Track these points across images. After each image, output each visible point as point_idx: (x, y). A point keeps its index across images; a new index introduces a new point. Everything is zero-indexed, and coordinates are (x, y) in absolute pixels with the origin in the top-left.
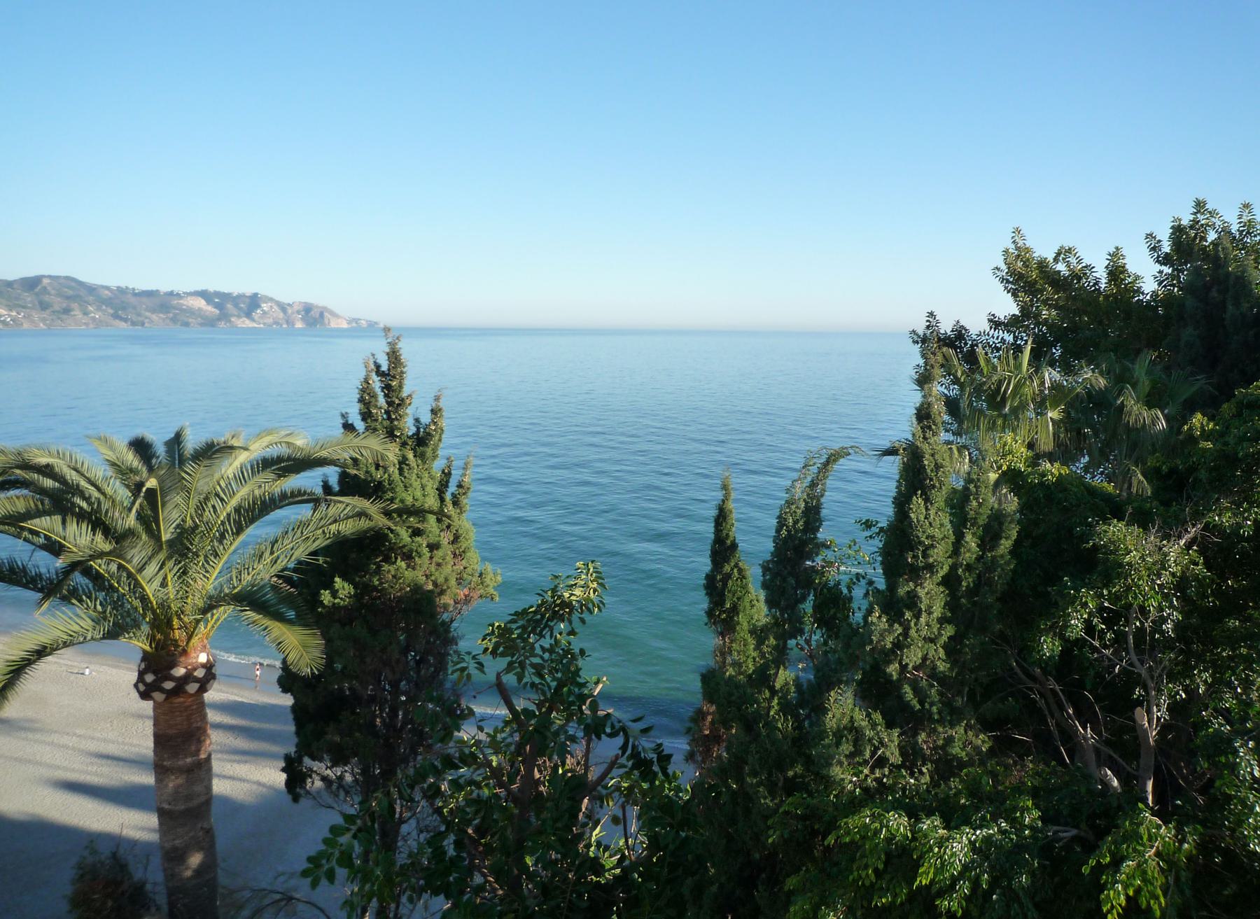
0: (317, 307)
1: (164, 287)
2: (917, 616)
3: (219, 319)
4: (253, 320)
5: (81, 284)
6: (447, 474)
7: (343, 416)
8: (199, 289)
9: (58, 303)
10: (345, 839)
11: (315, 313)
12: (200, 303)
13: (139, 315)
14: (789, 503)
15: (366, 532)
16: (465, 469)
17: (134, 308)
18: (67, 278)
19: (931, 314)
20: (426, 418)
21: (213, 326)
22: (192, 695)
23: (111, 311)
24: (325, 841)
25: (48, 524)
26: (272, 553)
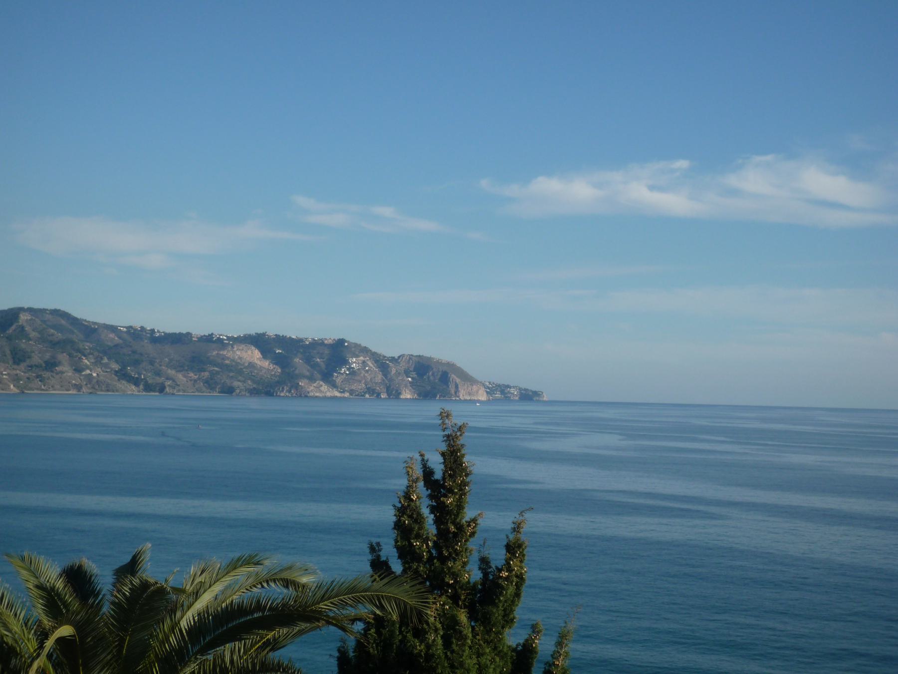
0: (439, 363)
1: (198, 327)
3: (280, 383)
4: (334, 385)
5: (75, 321)
8: (253, 331)
12: (253, 355)
13: (158, 373)
18: (56, 312)
20: (498, 556)
21: (269, 394)
23: (115, 366)
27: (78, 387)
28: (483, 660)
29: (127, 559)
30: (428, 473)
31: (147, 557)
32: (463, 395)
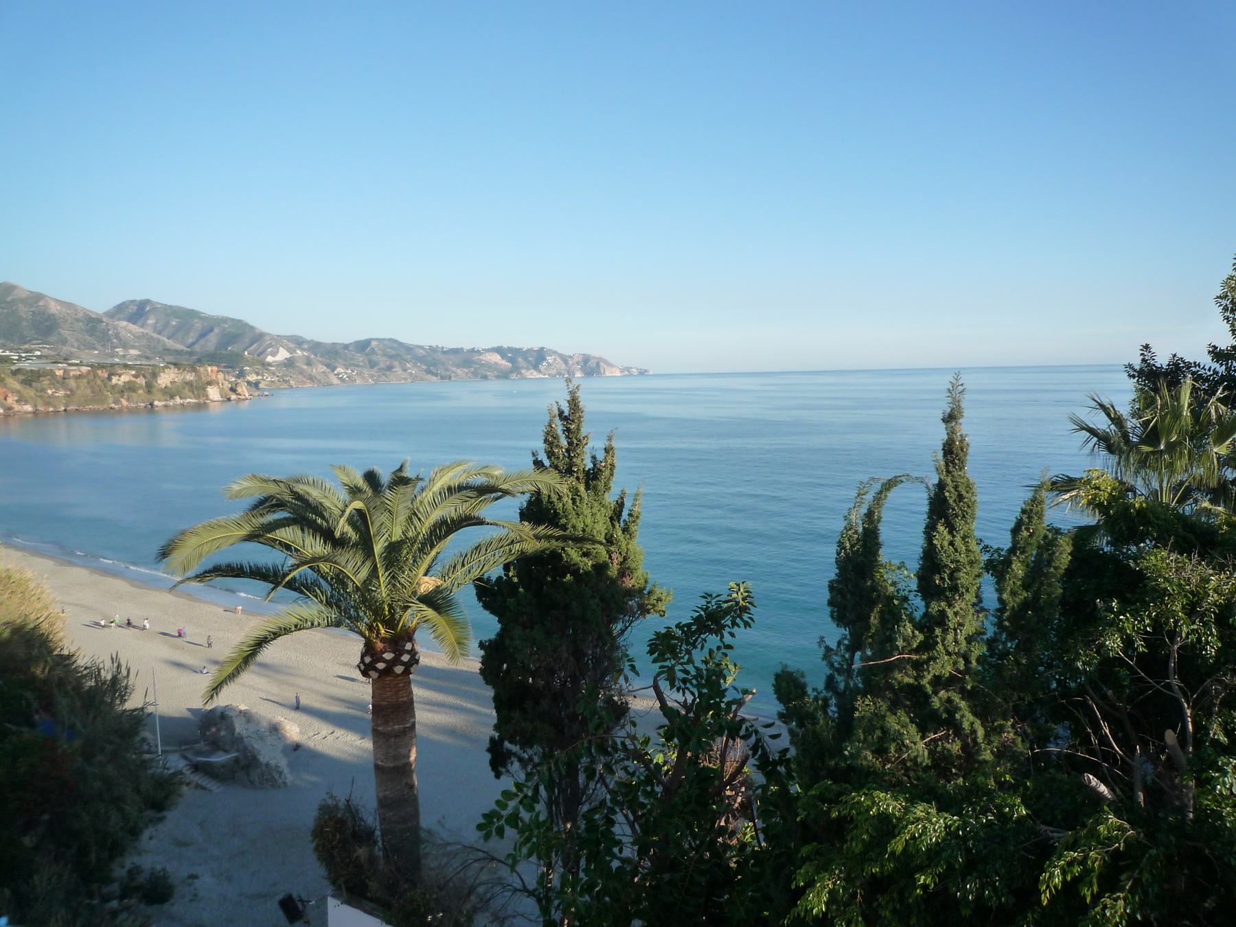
1: (467, 346)
2: (945, 631)
3: (512, 372)
6: (620, 505)
7: (533, 454)
8: (495, 345)
9: (383, 362)
10: (512, 804)
11: (592, 364)
12: (496, 358)
13: (447, 370)
14: (847, 529)
15: (543, 552)
16: (636, 500)
18: (390, 340)
19: (1147, 347)
20: (601, 456)
22: (398, 675)
24: (498, 802)
25: (288, 534)
26: (463, 565)
27: (405, 379)
28: (594, 510)
30: (561, 413)
31: (407, 465)
32: (607, 374)
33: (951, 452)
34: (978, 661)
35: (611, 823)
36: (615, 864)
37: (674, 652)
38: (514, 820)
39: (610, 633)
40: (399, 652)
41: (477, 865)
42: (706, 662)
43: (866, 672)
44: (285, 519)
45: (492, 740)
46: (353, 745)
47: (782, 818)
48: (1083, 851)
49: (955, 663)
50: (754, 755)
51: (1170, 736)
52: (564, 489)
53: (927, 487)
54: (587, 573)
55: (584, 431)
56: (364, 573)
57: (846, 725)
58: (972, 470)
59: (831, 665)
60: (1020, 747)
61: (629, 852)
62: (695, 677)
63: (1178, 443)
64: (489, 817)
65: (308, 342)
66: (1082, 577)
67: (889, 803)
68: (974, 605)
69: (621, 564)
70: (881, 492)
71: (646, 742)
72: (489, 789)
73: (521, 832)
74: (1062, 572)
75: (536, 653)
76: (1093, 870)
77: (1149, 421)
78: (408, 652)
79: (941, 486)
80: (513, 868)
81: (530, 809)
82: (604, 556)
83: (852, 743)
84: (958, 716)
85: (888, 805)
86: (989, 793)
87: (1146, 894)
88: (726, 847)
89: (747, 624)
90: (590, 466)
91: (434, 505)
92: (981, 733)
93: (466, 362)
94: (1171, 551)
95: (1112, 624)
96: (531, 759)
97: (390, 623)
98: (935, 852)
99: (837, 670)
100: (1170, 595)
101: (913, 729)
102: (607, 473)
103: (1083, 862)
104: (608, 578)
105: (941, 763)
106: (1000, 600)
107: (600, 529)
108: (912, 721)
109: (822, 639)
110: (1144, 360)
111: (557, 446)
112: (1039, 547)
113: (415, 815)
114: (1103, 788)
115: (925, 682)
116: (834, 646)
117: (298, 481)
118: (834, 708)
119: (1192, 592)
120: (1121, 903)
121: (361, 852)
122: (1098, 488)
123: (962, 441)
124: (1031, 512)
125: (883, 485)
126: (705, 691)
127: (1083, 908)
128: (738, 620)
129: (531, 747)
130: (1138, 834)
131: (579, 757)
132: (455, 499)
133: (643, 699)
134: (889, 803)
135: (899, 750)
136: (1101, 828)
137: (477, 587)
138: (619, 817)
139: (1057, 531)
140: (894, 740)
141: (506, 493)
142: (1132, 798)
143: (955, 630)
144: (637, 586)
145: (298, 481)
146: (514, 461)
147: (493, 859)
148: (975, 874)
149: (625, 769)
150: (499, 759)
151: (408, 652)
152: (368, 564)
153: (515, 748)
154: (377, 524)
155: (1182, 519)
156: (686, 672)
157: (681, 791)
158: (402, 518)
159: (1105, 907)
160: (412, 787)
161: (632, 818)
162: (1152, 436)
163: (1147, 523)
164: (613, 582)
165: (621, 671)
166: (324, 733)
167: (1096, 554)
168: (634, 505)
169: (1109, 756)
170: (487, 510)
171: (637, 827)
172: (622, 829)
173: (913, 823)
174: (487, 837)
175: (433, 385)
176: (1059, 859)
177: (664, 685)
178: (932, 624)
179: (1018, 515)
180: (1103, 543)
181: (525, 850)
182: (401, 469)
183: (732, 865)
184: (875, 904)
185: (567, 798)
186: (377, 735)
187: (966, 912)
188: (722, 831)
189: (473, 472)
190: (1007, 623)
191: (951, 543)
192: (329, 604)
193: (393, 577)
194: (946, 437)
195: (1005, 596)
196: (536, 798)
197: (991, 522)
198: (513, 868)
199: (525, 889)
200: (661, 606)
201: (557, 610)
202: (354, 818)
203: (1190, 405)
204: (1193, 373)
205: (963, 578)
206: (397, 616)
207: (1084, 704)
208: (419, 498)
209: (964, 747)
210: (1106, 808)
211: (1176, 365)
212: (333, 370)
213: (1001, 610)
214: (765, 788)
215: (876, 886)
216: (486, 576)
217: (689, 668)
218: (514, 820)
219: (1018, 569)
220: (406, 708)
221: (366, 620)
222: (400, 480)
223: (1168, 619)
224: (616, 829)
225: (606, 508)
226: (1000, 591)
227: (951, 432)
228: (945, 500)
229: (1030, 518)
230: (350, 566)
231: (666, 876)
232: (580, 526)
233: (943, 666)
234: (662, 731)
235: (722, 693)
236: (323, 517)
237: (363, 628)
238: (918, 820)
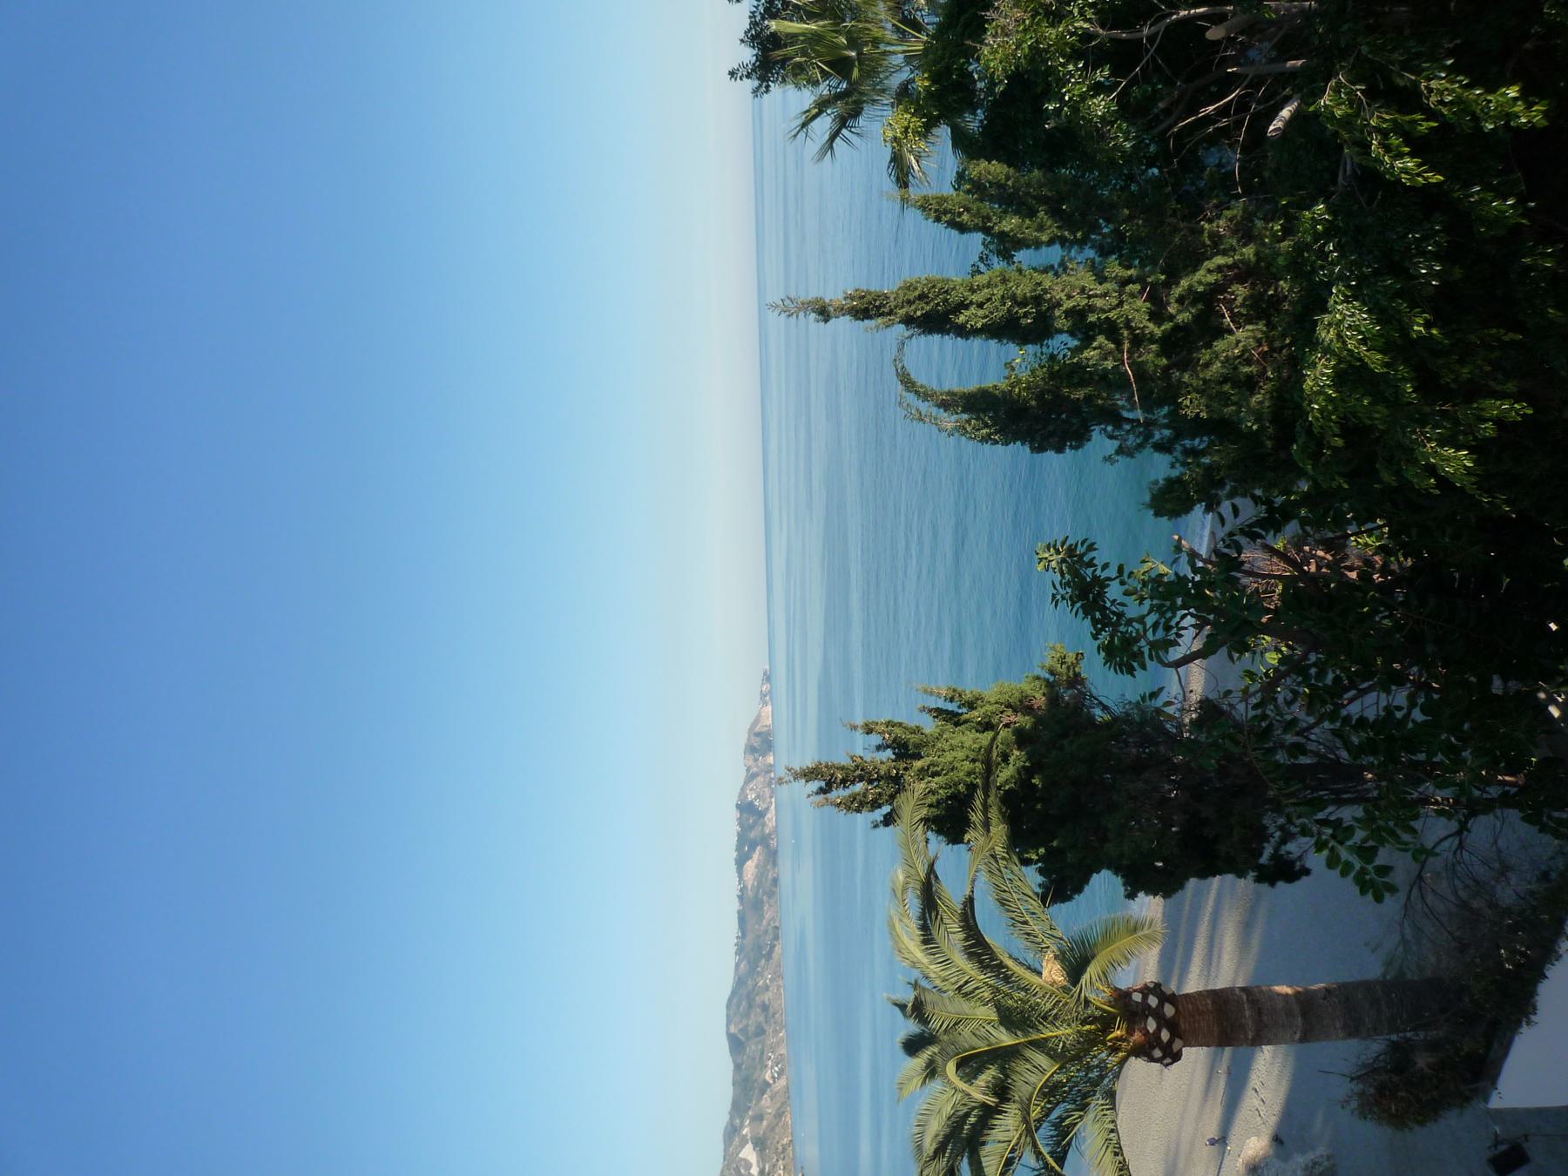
1: (735, 905)
2: (1091, 309)
3: (768, 846)
6: (938, 713)
7: (876, 826)
9: (757, 1017)
10: (1344, 854)
11: (756, 742)
12: (750, 866)
13: (766, 932)
15: (1003, 814)
16: (931, 693)
17: (758, 937)
18: (728, 1007)
19: (732, 74)
20: (875, 739)
21: (775, 852)
24: (1344, 874)
26: (1026, 923)
27: (779, 987)
29: (897, 1009)
30: (822, 791)
31: (894, 997)
33: (866, 310)
34: (1128, 268)
35: (1362, 722)
36: (1417, 715)
37: (1128, 642)
38: (1366, 853)
39: (1107, 725)
40: (1142, 1012)
41: (1430, 898)
42: (1142, 600)
43: (1148, 403)
44: (971, 1164)
45: (1258, 880)
46: (1269, 1069)
47: (1342, 501)
48: (1370, 134)
49: (1132, 295)
50: (1262, 537)
51: (1215, 33)
52: (920, 787)
53: (911, 337)
54: (1030, 757)
55: (845, 761)
56: (1041, 1059)
57: (1221, 428)
58: (887, 284)
59: (1140, 446)
60: (1237, 209)
61: (1401, 697)
62: (1162, 614)
63: (849, 34)
64: (1364, 885)
65: (732, 1119)
66: (1012, 138)
67: (1318, 375)
68: (1057, 275)
69: (1015, 711)
70: (917, 392)
71: (1251, 675)
72: (1324, 888)
73: (1382, 841)
74: (1012, 171)
75: (1138, 822)
76: (1394, 121)
77: (822, 71)
78: (1145, 997)
79: (908, 321)
80: (1431, 853)
81: (1350, 831)
82: (1004, 734)
83: (1240, 421)
84: (1200, 289)
85: (1323, 374)
86: (1300, 248)
87: (1418, 55)
88: (1384, 570)
89: (1091, 548)
90: (889, 753)
91: (947, 962)
92: (1220, 260)
93: (755, 905)
94: (982, 42)
95: (1075, 109)
96: (1281, 828)
97: (1106, 1023)
98: (1380, 313)
99: (1146, 439)
100: (1037, 42)
101: (1219, 345)
102: (898, 731)
103: (1385, 134)
104: (1035, 725)
105: (1261, 309)
106: (1051, 242)
107: (970, 739)
108: (1209, 345)
109: (1108, 459)
110: (748, 76)
111: (865, 795)
112: (981, 200)
113: (1366, 986)
114: (1286, 113)
115: (1158, 332)
116: (1116, 443)
117: (919, 1147)
118: (1197, 441)
119: (1033, 17)
120: (1434, 84)
121: (1422, 1061)
122: (907, 128)
123: (852, 298)
124: (938, 211)
125: (908, 390)
126: (1179, 601)
127: (1445, 128)
128: (1086, 559)
129: (1266, 828)
130: (1342, 68)
131: (1278, 765)
132: (938, 935)
133: (1189, 683)
134: (1318, 375)
135: (1249, 362)
136: (1338, 113)
137: (1054, 901)
138: (1354, 709)
139: (961, 176)
140: (1236, 368)
141: (931, 870)
142: (1294, 74)
143: (1089, 297)
144: (1044, 690)
145: (919, 1148)
146: (886, 854)
147: (1420, 877)
148: (1407, 264)
149: (1289, 703)
150: (1285, 871)
151: (1145, 997)
152: (1029, 1053)
153: (1268, 851)
154: (975, 1041)
155: (942, 29)
156: (1155, 626)
157: (1314, 631)
158: (965, 1007)
159: (1441, 102)
160: (1328, 991)
161: (1353, 692)
162: (840, 66)
163: (948, 70)
164: (1039, 721)
165: (1158, 711)
166: (1256, 1102)
167: (986, 129)
168: (939, 695)
169: (1242, 105)
170: (952, 892)
171: (1365, 685)
172: (1368, 705)
173: (1344, 343)
174: (1392, 889)
175: (785, 951)
176: (1382, 162)
177: (1176, 654)
178: (1083, 325)
179: (941, 226)
180: (973, 122)
181: (1406, 837)
182: (902, 1007)
183: (1409, 562)
184: (1453, 386)
185: (1333, 779)
186: (1258, 1040)
187: (1458, 273)
188: (1365, 576)
189: (901, 909)
190: (1079, 235)
191: (980, 305)
192: (1084, 1107)
193: (1045, 1018)
194: (848, 317)
195: (1045, 238)
196: (1337, 824)
197: (951, 258)
198: (1431, 853)
199: (1459, 833)
200: (1071, 658)
201: (1075, 794)
202: (1375, 1070)
203: (802, 20)
204: (763, 19)
205: (1023, 289)
206: (1098, 1013)
207: (1178, 136)
208: (938, 982)
209: (1240, 279)
210: (1312, 109)
211: (753, 38)
212: (768, 1085)
213: (1063, 241)
214: (1304, 522)
215: (1428, 384)
216: (1040, 891)
217: (1150, 620)
218: (1366, 853)
219: (1010, 224)
220: (1220, 1001)
221: (1103, 1055)
222: (918, 1010)
223: (1067, 44)
224: (1371, 715)
225: (943, 731)
226: (1037, 244)
227: (842, 311)
228: (926, 316)
229: (945, 212)
230: (1033, 1078)
231: (1430, 648)
232: (967, 765)
233: (1137, 310)
234: (1236, 655)
235: (1181, 580)
236: (967, 1115)
237: (1113, 1060)
238: (1339, 336)
